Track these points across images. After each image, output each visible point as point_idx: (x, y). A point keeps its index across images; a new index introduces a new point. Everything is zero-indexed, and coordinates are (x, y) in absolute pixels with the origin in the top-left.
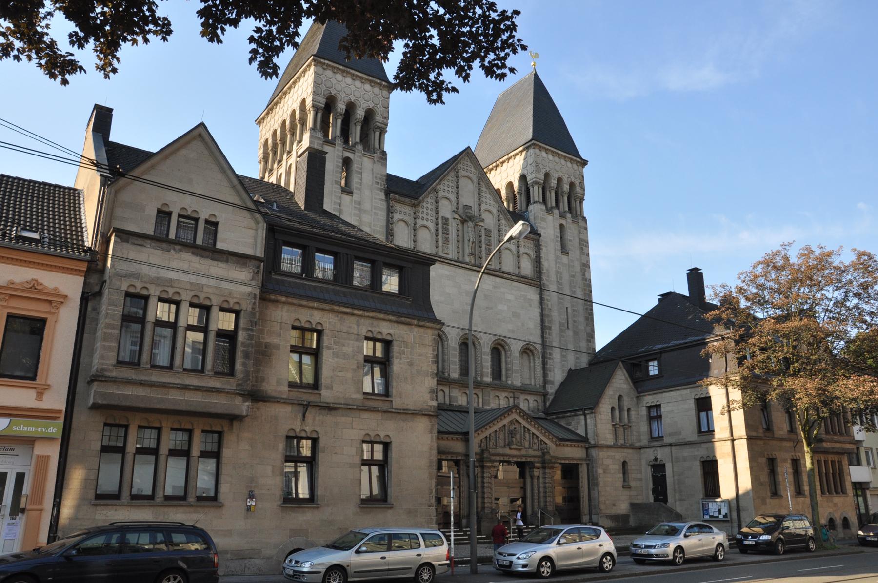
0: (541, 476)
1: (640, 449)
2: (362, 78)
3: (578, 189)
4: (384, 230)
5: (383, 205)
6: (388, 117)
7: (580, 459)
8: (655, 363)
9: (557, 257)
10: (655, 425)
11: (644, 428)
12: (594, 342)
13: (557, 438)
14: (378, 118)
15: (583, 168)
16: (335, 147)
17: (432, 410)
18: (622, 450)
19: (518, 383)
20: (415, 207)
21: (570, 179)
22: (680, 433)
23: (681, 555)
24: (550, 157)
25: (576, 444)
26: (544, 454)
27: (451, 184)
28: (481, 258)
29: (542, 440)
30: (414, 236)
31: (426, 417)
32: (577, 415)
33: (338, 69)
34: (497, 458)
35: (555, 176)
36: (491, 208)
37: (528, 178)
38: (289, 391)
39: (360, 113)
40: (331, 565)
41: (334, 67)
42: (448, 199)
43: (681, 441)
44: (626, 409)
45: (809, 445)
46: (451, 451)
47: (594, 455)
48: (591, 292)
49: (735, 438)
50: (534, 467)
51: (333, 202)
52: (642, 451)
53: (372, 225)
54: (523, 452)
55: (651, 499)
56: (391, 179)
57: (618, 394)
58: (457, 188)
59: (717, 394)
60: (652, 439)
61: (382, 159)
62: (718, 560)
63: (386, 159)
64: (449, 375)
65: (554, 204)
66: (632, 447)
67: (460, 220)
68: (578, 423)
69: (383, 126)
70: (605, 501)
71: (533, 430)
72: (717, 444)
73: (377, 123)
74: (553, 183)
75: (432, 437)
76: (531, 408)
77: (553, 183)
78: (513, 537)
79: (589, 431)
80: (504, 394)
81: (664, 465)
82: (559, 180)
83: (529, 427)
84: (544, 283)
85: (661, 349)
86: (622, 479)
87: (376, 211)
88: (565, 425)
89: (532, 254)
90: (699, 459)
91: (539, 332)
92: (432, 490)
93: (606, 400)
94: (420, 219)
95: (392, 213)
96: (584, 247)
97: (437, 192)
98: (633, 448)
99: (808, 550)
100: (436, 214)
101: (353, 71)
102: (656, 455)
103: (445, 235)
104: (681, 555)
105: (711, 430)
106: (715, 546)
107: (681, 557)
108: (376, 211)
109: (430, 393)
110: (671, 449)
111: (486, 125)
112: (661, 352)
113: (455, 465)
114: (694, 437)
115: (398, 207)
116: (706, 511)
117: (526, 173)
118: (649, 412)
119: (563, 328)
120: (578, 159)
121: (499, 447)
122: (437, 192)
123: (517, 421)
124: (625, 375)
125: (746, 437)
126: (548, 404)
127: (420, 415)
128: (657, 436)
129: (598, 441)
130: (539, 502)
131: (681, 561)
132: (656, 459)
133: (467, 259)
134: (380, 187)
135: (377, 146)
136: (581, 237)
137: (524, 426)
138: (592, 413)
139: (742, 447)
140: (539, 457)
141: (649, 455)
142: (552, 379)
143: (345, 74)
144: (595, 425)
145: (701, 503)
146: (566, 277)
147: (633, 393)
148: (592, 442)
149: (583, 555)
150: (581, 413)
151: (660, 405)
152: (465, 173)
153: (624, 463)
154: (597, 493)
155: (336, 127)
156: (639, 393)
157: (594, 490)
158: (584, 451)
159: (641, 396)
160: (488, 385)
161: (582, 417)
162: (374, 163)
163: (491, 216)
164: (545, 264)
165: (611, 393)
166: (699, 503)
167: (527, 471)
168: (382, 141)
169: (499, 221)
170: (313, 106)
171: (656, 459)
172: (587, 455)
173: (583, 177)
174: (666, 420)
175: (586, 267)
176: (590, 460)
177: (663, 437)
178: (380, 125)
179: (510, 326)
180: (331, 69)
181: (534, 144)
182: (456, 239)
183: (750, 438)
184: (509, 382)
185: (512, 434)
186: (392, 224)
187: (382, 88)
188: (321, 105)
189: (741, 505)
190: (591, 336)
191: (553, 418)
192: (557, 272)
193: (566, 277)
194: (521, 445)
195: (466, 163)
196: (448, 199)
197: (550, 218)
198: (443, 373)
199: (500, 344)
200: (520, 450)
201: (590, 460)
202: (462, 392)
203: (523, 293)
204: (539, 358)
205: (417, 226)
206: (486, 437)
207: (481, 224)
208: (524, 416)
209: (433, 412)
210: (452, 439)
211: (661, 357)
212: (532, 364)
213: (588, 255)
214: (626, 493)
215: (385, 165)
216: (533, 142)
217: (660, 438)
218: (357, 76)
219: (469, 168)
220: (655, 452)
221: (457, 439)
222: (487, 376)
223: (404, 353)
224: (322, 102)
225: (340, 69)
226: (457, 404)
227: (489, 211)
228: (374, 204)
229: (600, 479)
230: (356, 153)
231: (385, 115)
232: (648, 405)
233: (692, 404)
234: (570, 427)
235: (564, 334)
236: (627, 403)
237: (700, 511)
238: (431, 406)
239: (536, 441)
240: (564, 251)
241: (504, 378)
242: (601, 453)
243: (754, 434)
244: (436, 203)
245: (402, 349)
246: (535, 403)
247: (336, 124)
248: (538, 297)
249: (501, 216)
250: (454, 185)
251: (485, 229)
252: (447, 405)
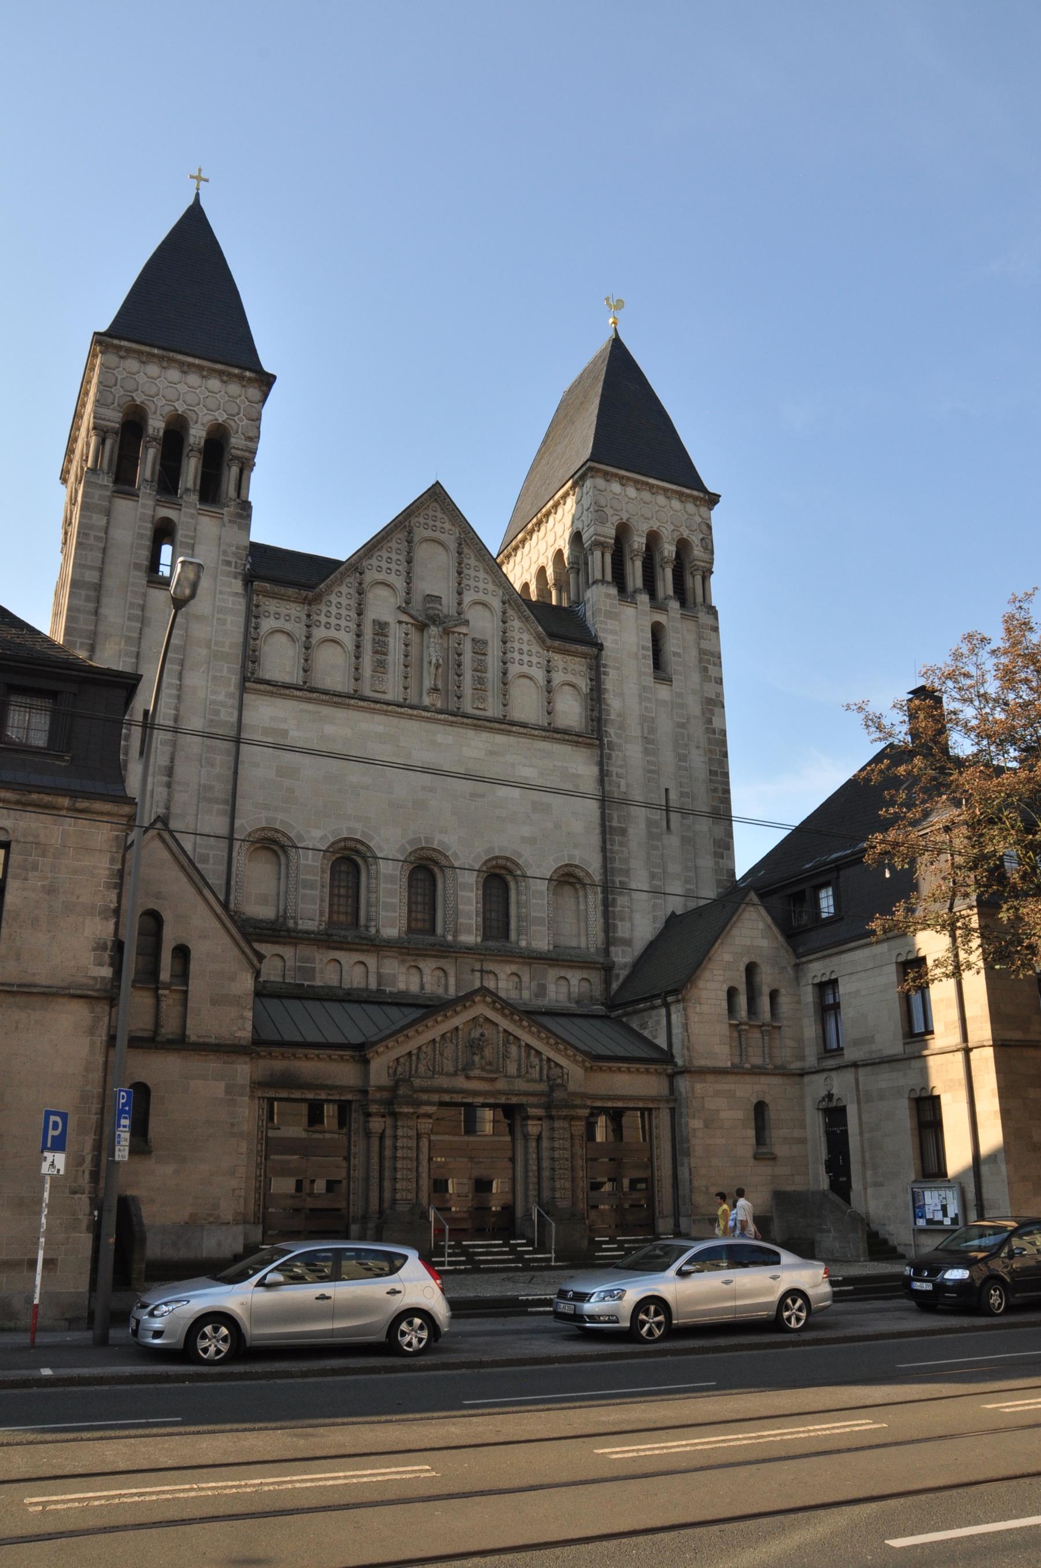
0: (545, 1134)
1: (802, 1075)
2: (200, 368)
3: (697, 552)
4: (239, 651)
5: (241, 605)
6: (258, 437)
8: (830, 891)
11: (810, 1030)
12: (731, 858)
13: (584, 1053)
14: (236, 441)
16: (138, 501)
17: (98, 986)
18: (756, 1079)
19: (542, 943)
20: (309, 604)
22: (871, 1040)
23: (661, 1318)
24: (631, 492)
25: (642, 1067)
26: (552, 1089)
27: (394, 556)
28: (459, 698)
29: (549, 1060)
30: (306, 660)
31: (81, 1001)
33: (149, 354)
34: (435, 1098)
36: (488, 599)
37: (585, 537)
39: (197, 434)
40: (395, 1315)
41: (140, 353)
42: (388, 585)
43: (874, 1056)
44: (766, 990)
46: (329, 1082)
47: (682, 1089)
48: (725, 755)
50: (528, 1118)
51: (128, 603)
53: (213, 644)
54: (501, 1085)
56: (259, 551)
57: (746, 960)
58: (409, 562)
61: (240, 516)
62: (988, 1312)
63: (249, 517)
64: (378, 931)
65: (639, 583)
66: (781, 1072)
67: (412, 624)
68: (658, 1023)
69: (247, 454)
70: (707, 1188)
71: (527, 1038)
72: (933, 1062)
73: (233, 451)
74: (638, 542)
75: (92, 1044)
76: (575, 995)
77: (638, 542)
78: (450, 1263)
80: (510, 969)
81: (843, 1109)
82: (653, 538)
83: (518, 1032)
84: (609, 742)
86: (754, 1141)
87: (221, 616)
88: (637, 1029)
89: (584, 684)
90: (906, 1095)
91: (595, 839)
92: (84, 1157)
93: (715, 972)
94: (322, 627)
95: (257, 617)
96: (710, 667)
97: (361, 574)
98: (783, 1075)
100: (359, 615)
101: (180, 357)
102: (829, 1088)
103: (378, 656)
104: (661, 1318)
106: (775, 1297)
107: (659, 1324)
108: (221, 616)
109: (95, 949)
110: (856, 1074)
111: (539, 451)
112: (837, 866)
113: (506, 1117)
115: (271, 605)
116: (918, 1210)
119: (655, 830)
120: (696, 493)
121: (441, 1073)
122: (361, 574)
123: (487, 1019)
126: (615, 986)
127: (64, 996)
129: (690, 1061)
130: (539, 1190)
131: (658, 1333)
132: (830, 1096)
133: (427, 701)
134: (233, 569)
135: (232, 493)
136: (702, 646)
137: (505, 1031)
138: (678, 1001)
139: (985, 1061)
140: (541, 1094)
141: (816, 1087)
142: (626, 935)
143: (165, 364)
144: (686, 1027)
145: (910, 1191)
147: (787, 958)
148: (680, 1062)
149: (333, 1314)
150: (659, 1002)
151: (835, 981)
152: (428, 533)
153: (760, 1109)
154: (687, 1170)
156: (798, 956)
157: (682, 1165)
158: (665, 1083)
159: (803, 963)
160: (469, 950)
163: (487, 613)
164: (614, 703)
165: (727, 957)
167: (518, 1123)
168: (243, 485)
169: (504, 622)
170: (94, 428)
172: (672, 1089)
173: (710, 528)
174: (847, 1012)
175: (715, 705)
177: (842, 1049)
178: (239, 453)
179: (526, 831)
180: (177, 366)
182: (402, 661)
183: (1002, 1045)
184: (523, 944)
185: (475, 1046)
186: (255, 639)
188: (113, 424)
189: (985, 1196)
190: (725, 846)
191: (619, 1016)
192: (643, 719)
193: (665, 726)
194: (497, 1071)
195: (431, 513)
196: (388, 585)
197: (629, 611)
198: (367, 927)
199: (504, 868)
200: (493, 1080)
202: (407, 965)
203: (559, 764)
204: (596, 893)
205: (314, 641)
206: (410, 1054)
207: (464, 630)
208: (503, 1008)
209: (97, 991)
210: (330, 1057)
211: (838, 877)
212: (582, 907)
213: (720, 681)
214: (765, 1170)
215: (247, 528)
218: (190, 365)
219: (438, 524)
221: (341, 1057)
222: (469, 932)
223: (35, 867)
224: (114, 418)
225: (153, 355)
226: (395, 990)
227: (484, 604)
228: (217, 603)
229: (693, 1141)
230: (183, 509)
231: (251, 434)
232: (817, 981)
233: (891, 973)
234: (646, 1033)
235: (659, 844)
236: (766, 979)
238: (95, 978)
239: (535, 1061)
241: (513, 936)
243: (1017, 1035)
244: (360, 594)
245: (31, 859)
246: (585, 984)
248: (595, 770)
249: (510, 612)
250: (402, 558)
251: (473, 640)
252: (371, 991)
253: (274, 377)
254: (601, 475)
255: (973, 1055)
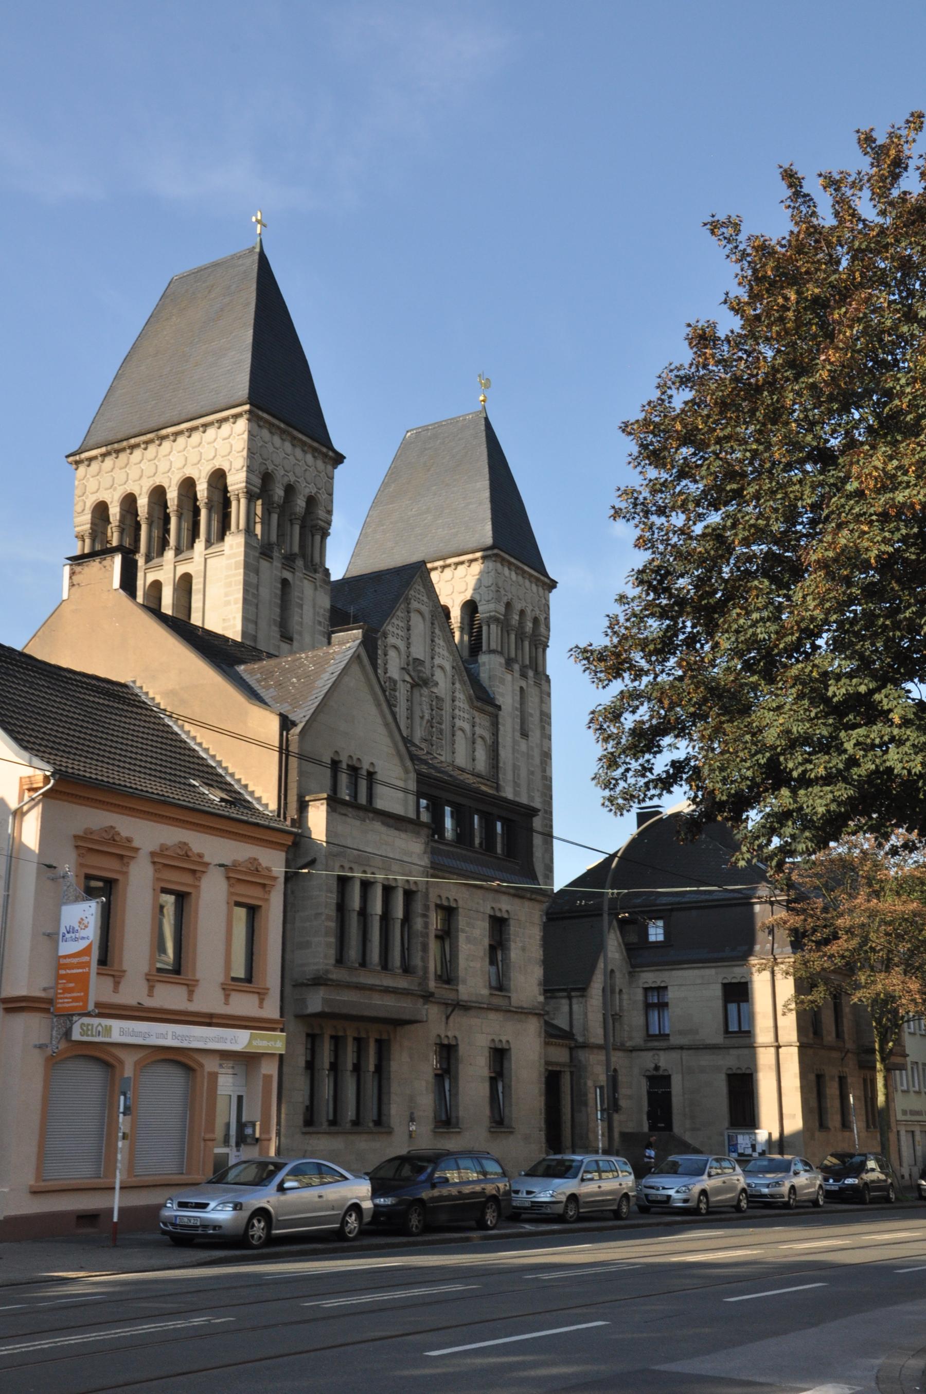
1: (631, 1051)
2: (304, 443)
7: (563, 1065)
9: (515, 742)
10: (654, 1016)
15: (550, 592)
21: (264, 467)
32: (556, 998)
35: (518, 606)
38: (491, 994)
44: (617, 990)
45: (883, 1060)
47: (582, 1059)
49: (781, 1044)
52: (634, 1054)
55: (646, 1129)
59: (760, 983)
60: (650, 1037)
62: (700, 1214)
73: (320, 522)
79: (575, 1023)
85: (672, 904)
99: (887, 1200)
105: (745, 1028)
114: (719, 1039)
117: (477, 598)
118: (646, 996)
124: (618, 941)
125: (798, 1044)
128: (657, 1032)
132: (657, 1068)
141: (647, 1060)
144: (586, 1014)
146: (523, 773)
148: (580, 1039)
150: (565, 994)
151: (666, 988)
155: (269, 525)
156: (633, 966)
161: (565, 1002)
162: (316, 589)
166: (722, 1134)
171: (657, 1068)
176: (575, 1066)
181: (496, 555)
187: (306, 448)
201: (575, 1066)
216: (496, 551)
217: (664, 1036)
220: (656, 1057)
230: (297, 573)
232: (646, 986)
233: (717, 991)
236: (620, 980)
237: (724, 1146)
240: (524, 734)
242: (591, 1057)
247: (269, 520)
249: (456, 677)
253: (345, 458)
254: (267, 426)
255: (781, 1050)
